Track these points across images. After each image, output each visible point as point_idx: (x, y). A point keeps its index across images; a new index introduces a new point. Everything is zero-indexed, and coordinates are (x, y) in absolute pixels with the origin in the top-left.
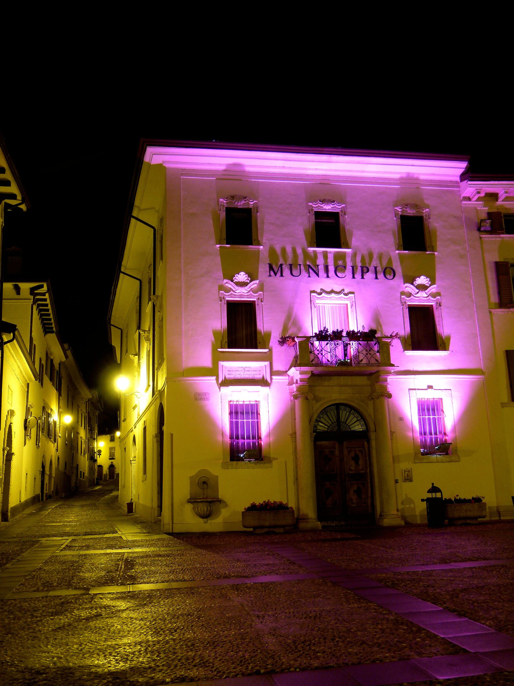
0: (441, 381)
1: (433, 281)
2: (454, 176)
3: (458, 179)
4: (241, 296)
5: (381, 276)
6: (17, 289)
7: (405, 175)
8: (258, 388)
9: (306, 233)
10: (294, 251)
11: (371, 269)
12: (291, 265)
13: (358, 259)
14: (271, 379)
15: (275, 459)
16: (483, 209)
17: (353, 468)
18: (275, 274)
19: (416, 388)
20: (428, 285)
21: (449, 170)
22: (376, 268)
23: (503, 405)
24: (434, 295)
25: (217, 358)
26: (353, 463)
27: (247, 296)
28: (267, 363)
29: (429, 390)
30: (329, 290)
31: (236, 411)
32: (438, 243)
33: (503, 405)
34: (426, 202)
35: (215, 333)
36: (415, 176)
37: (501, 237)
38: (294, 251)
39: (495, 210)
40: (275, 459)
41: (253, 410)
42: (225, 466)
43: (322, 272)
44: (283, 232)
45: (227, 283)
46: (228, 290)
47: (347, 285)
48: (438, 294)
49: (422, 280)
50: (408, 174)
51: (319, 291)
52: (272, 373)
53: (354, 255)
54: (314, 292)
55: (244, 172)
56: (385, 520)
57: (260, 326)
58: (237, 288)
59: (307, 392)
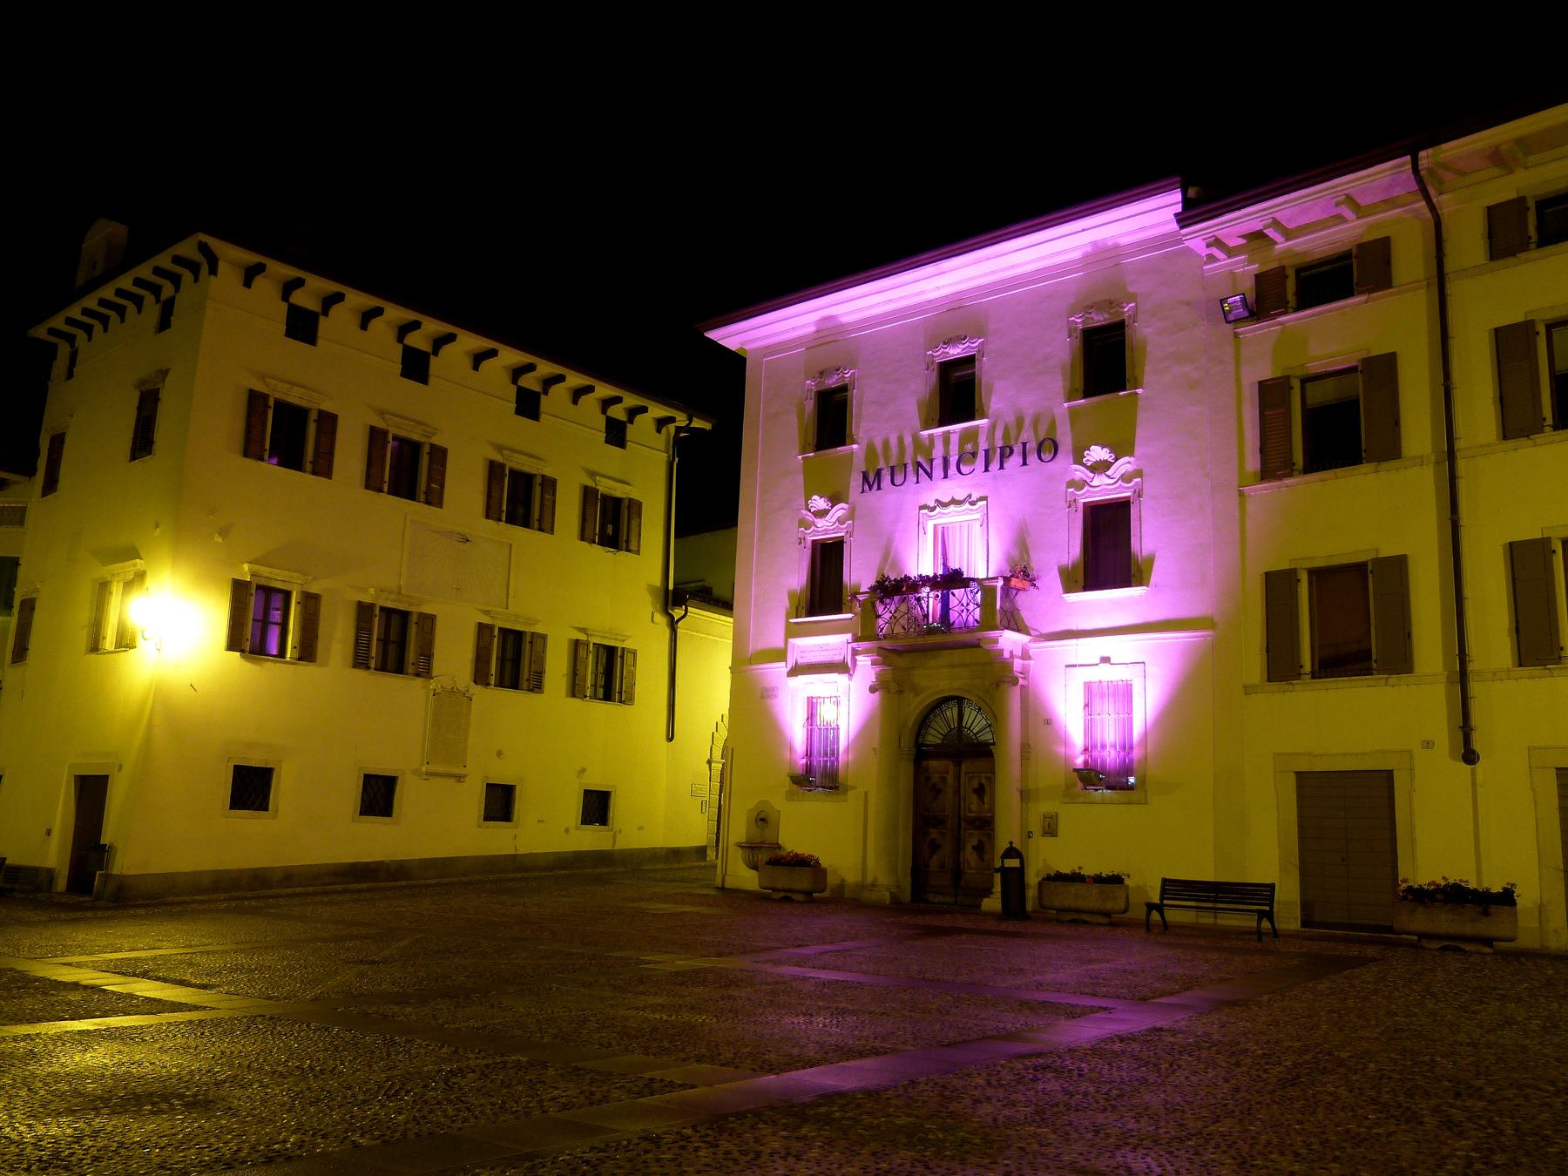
0: (1125, 648)
2: (1166, 223)
3: (1175, 226)
4: (826, 531)
5: (1032, 458)
7: (1089, 249)
8: (834, 676)
9: (920, 405)
10: (901, 441)
11: (1018, 449)
12: (893, 468)
13: (999, 434)
15: (853, 788)
16: (1245, 269)
17: (974, 807)
18: (871, 488)
21: (1146, 219)
22: (1024, 444)
23: (1248, 690)
24: (1126, 478)
26: (974, 797)
30: (946, 500)
32: (1147, 368)
33: (1248, 690)
34: (1131, 289)
35: (791, 595)
36: (1110, 243)
37: (1280, 324)
38: (901, 441)
39: (1275, 265)
40: (853, 788)
42: (790, 796)
43: (938, 471)
44: (889, 413)
47: (976, 486)
48: (1138, 473)
49: (1097, 453)
50: (1094, 244)
51: (932, 504)
53: (993, 427)
54: (924, 507)
55: (842, 325)
56: (985, 900)
57: (846, 579)
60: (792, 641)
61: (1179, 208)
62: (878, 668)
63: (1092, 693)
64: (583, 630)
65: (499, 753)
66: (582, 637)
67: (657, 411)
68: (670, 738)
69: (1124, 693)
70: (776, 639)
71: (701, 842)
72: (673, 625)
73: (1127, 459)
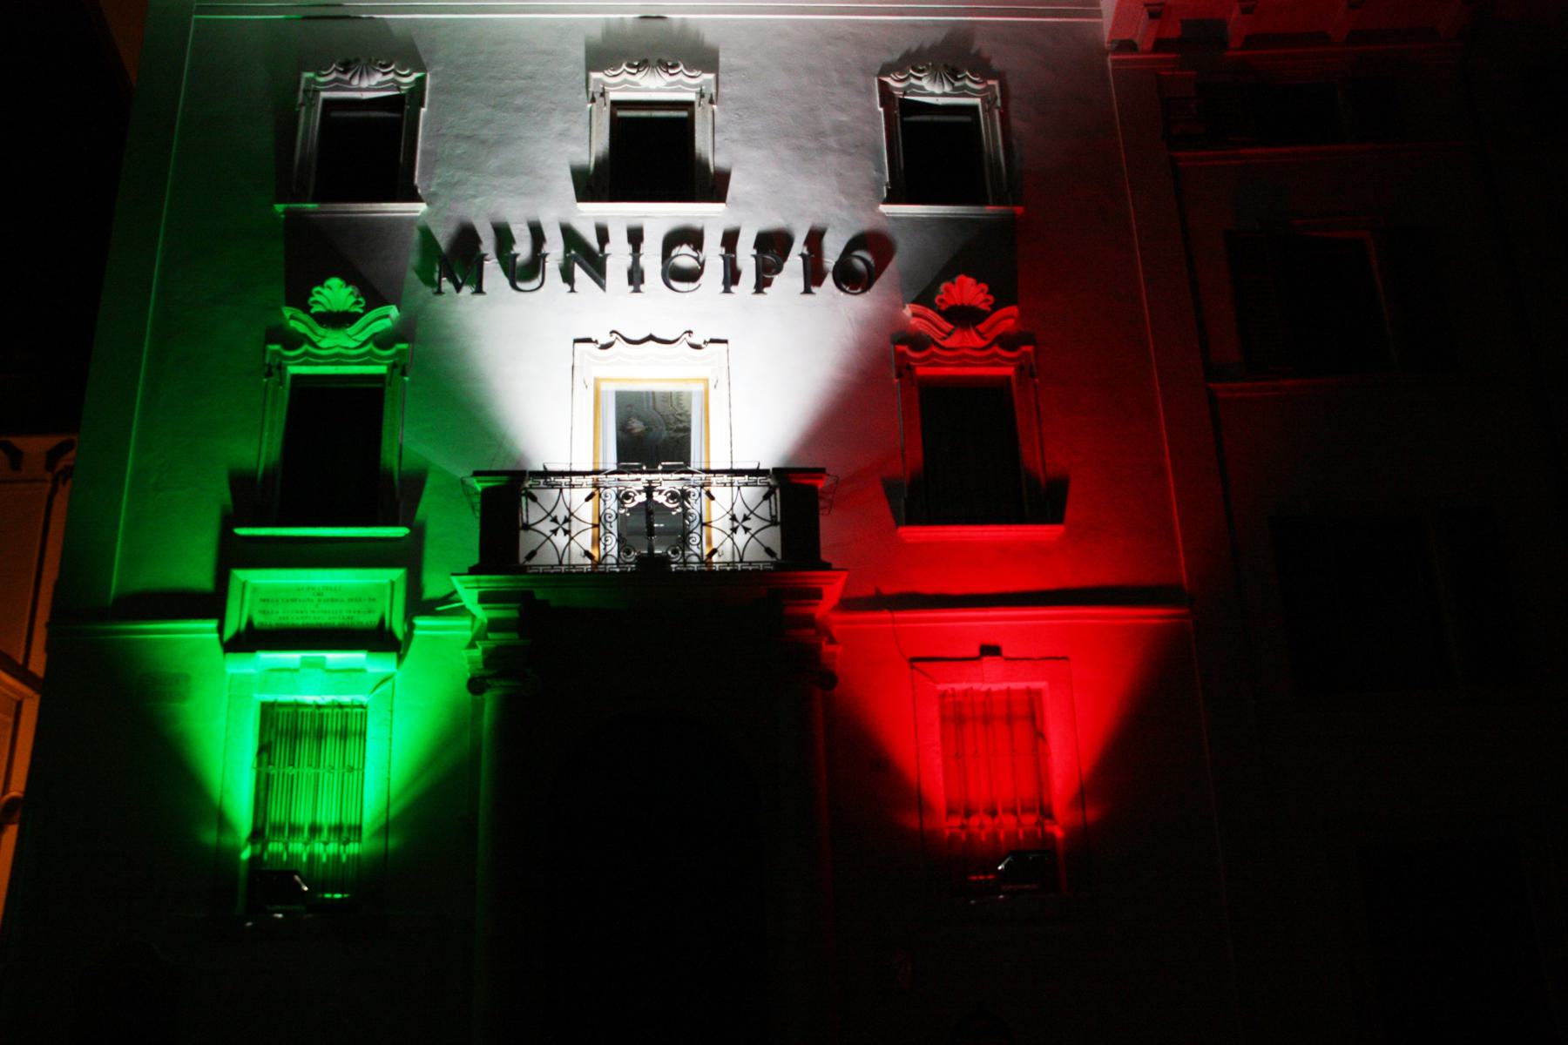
1: (1003, 294)
4: (338, 359)
8: (357, 657)
14: (411, 627)
19: (576, 468)
20: (983, 307)
27: (358, 356)
28: (398, 574)
29: (986, 659)
45: (292, 318)
52: (418, 605)
57: (389, 458)
58: (321, 331)
59: (505, 668)
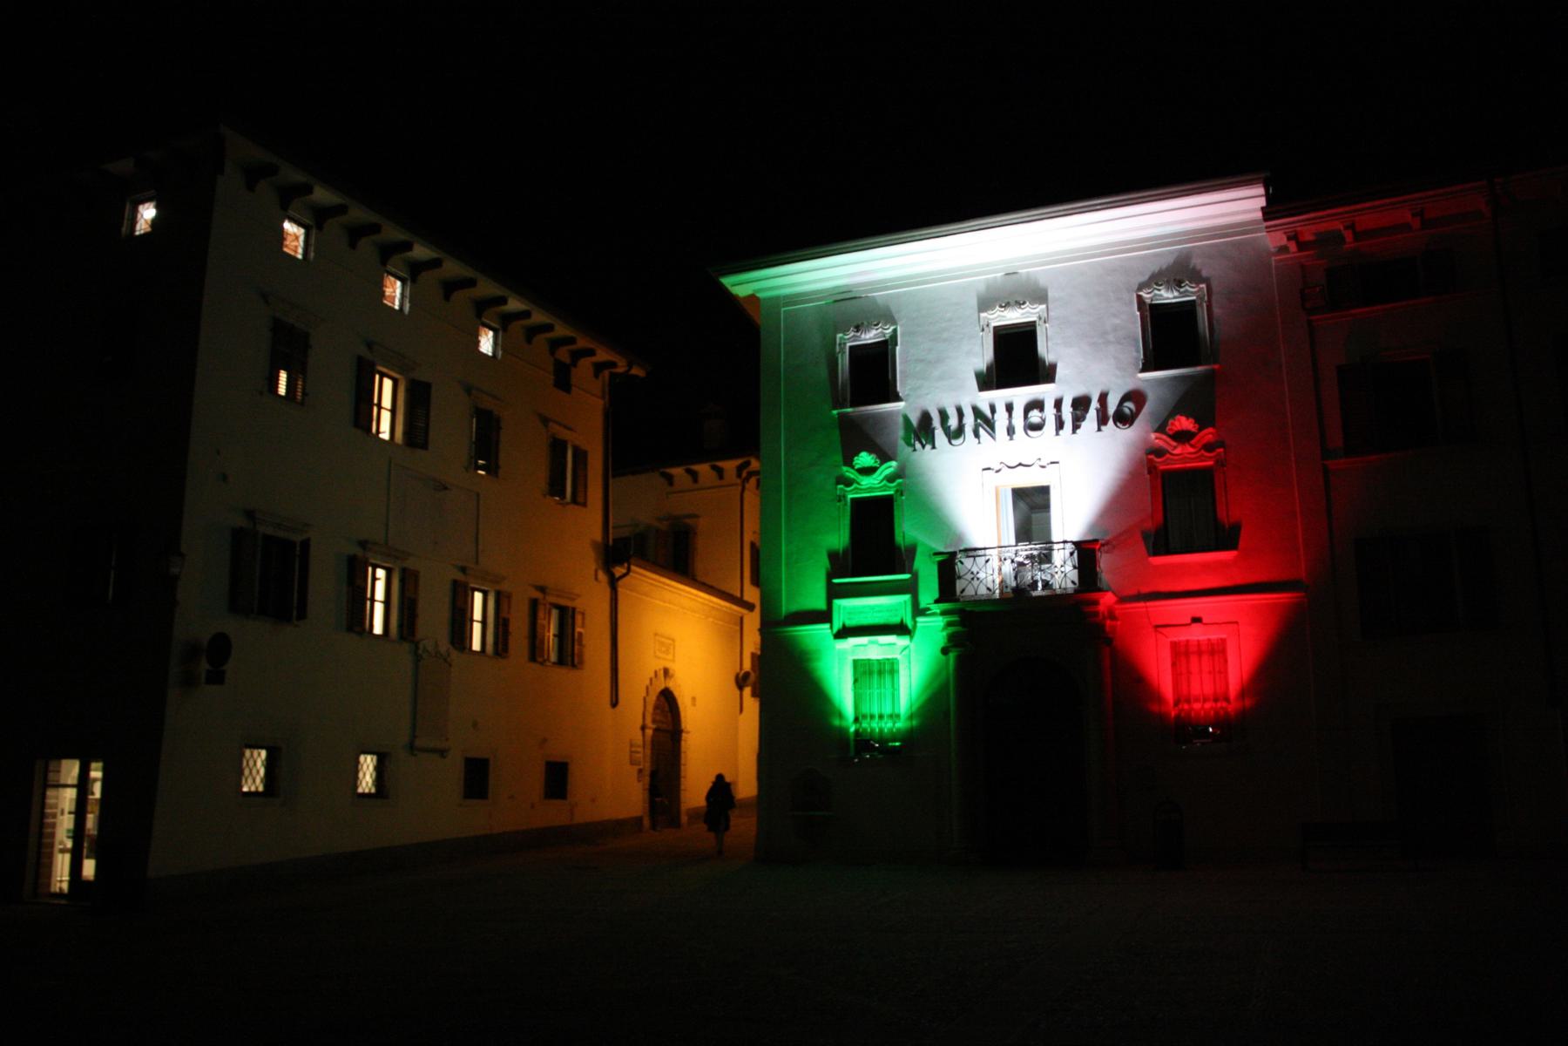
1: (1202, 423)
2: (1255, 210)
4: (871, 489)
6: (720, 472)
25: (834, 592)
28: (907, 597)
31: (864, 671)
41: (887, 669)
46: (848, 483)
57: (899, 538)
60: (837, 603)
61: (1262, 202)
62: (951, 630)
63: (1180, 652)
64: (542, 589)
65: (475, 725)
66: (538, 595)
67: (603, 355)
68: (615, 704)
69: (1217, 650)
70: (815, 599)
71: (639, 814)
72: (613, 583)
73: (1210, 430)
